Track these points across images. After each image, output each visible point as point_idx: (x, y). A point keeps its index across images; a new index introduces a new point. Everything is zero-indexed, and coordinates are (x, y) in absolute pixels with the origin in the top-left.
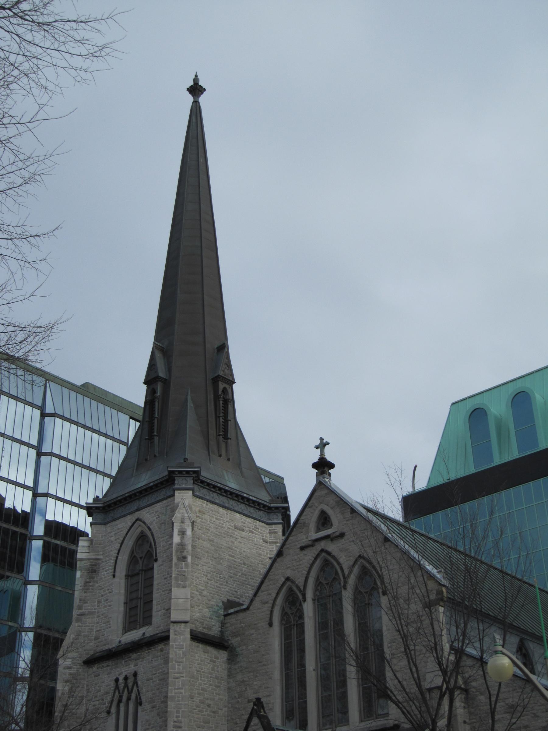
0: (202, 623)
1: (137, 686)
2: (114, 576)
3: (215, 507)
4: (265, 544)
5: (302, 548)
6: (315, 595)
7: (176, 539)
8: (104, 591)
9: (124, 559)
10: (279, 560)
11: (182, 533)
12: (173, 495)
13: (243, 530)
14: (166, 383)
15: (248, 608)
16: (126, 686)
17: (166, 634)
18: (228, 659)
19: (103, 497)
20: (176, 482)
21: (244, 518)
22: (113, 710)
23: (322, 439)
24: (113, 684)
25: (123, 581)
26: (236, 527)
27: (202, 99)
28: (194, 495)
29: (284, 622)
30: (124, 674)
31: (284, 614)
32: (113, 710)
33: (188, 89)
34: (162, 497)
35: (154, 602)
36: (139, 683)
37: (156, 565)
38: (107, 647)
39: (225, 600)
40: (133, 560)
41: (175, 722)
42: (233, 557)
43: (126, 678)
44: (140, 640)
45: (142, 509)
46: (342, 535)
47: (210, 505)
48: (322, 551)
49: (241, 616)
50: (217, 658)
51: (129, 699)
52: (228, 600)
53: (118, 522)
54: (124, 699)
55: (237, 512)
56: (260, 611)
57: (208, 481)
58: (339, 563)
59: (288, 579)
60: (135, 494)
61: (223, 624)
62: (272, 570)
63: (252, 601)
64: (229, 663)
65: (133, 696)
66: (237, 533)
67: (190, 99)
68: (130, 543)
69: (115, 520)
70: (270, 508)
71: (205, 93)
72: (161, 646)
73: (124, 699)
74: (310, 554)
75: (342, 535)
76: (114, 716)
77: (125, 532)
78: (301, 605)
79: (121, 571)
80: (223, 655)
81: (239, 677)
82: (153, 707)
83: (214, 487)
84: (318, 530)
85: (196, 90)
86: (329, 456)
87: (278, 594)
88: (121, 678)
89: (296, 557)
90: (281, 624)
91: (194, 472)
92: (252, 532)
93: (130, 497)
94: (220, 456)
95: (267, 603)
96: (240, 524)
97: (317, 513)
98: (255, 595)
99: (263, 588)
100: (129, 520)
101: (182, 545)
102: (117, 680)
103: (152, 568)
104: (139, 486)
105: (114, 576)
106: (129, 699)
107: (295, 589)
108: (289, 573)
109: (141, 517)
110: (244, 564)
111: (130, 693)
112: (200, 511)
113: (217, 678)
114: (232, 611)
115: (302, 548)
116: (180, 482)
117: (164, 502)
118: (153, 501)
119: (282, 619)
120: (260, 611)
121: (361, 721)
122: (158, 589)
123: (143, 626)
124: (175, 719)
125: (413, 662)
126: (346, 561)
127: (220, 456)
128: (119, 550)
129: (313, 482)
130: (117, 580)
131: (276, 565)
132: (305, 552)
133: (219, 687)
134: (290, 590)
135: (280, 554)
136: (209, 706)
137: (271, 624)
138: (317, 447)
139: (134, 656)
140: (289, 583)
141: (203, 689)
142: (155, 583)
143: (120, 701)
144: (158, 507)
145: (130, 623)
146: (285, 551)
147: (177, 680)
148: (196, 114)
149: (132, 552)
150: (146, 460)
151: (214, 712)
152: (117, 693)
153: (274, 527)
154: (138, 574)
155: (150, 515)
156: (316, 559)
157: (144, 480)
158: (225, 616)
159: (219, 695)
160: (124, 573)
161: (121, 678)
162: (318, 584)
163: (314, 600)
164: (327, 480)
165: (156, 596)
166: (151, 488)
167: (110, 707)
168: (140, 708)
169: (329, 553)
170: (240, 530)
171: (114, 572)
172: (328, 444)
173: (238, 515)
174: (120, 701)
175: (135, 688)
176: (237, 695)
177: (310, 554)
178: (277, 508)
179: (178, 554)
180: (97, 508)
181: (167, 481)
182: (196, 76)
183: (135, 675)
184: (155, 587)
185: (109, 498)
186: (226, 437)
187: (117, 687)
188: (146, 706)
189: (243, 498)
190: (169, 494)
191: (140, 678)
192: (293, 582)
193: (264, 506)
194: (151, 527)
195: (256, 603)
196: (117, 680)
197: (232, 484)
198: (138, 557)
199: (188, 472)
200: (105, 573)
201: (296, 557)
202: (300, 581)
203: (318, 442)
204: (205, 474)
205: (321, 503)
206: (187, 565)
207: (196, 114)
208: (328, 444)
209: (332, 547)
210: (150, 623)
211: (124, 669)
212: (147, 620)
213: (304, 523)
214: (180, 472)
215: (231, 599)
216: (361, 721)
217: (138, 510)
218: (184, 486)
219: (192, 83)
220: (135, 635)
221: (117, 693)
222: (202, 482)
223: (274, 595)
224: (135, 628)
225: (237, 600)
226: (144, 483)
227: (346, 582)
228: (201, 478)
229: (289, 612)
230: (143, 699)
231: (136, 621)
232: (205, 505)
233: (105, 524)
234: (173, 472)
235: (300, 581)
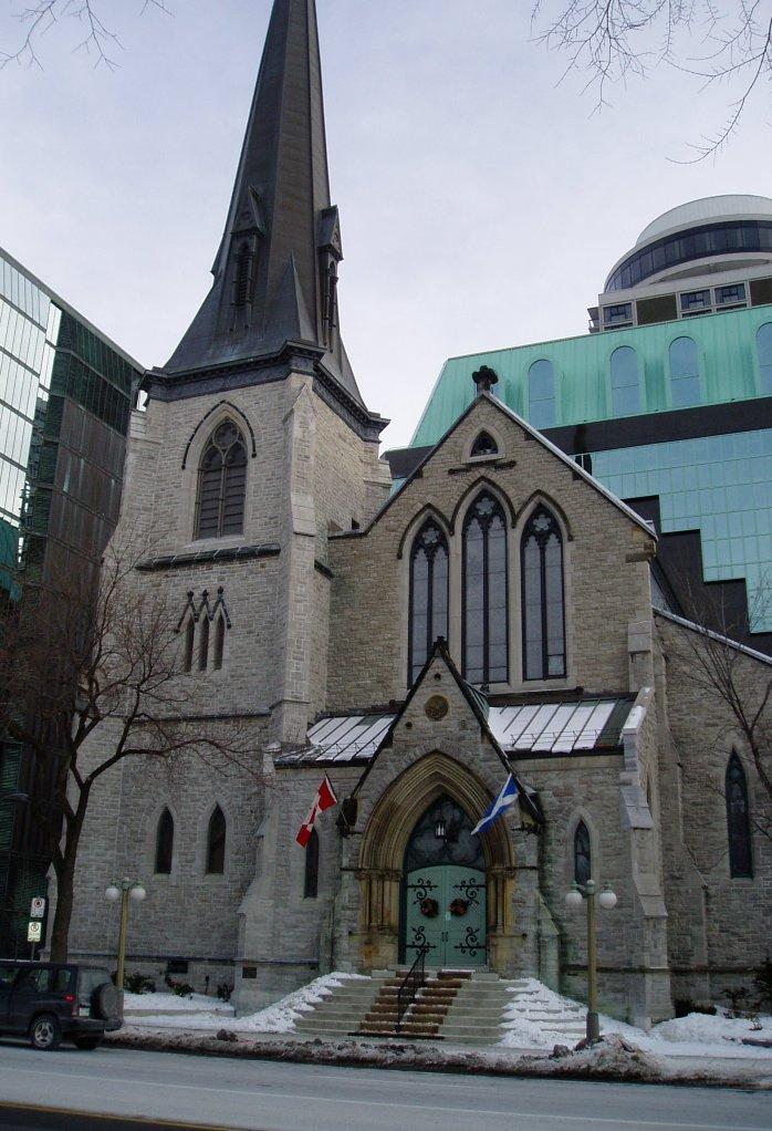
2: (183, 467)
5: (452, 472)
8: (167, 484)
9: (197, 449)
14: (264, 240)
15: (364, 534)
16: (205, 602)
32: (183, 629)
34: (264, 379)
36: (226, 602)
43: (205, 594)
45: (739, 268)
46: (512, 464)
56: (383, 540)
59: (429, 506)
63: (372, 525)
64: (332, 595)
74: (463, 482)
75: (512, 464)
76: (184, 636)
79: (194, 463)
81: (348, 613)
82: (249, 632)
84: (474, 453)
87: (412, 522)
88: (197, 594)
93: (212, 372)
96: (342, 433)
97: (476, 432)
98: (378, 519)
100: (216, 399)
102: (191, 595)
108: (430, 499)
115: (452, 472)
116: (296, 363)
118: (249, 381)
120: (383, 540)
124: (296, 650)
129: (472, 396)
130: (186, 473)
137: (400, 556)
147: (299, 604)
150: (231, 330)
156: (471, 487)
160: (196, 466)
161: (197, 594)
166: (248, 364)
171: (184, 462)
177: (463, 482)
180: (160, 379)
183: (221, 591)
185: (644, 239)
191: (225, 596)
194: (245, 413)
209: (494, 475)
212: (235, 524)
221: (190, 610)
233: (167, 401)
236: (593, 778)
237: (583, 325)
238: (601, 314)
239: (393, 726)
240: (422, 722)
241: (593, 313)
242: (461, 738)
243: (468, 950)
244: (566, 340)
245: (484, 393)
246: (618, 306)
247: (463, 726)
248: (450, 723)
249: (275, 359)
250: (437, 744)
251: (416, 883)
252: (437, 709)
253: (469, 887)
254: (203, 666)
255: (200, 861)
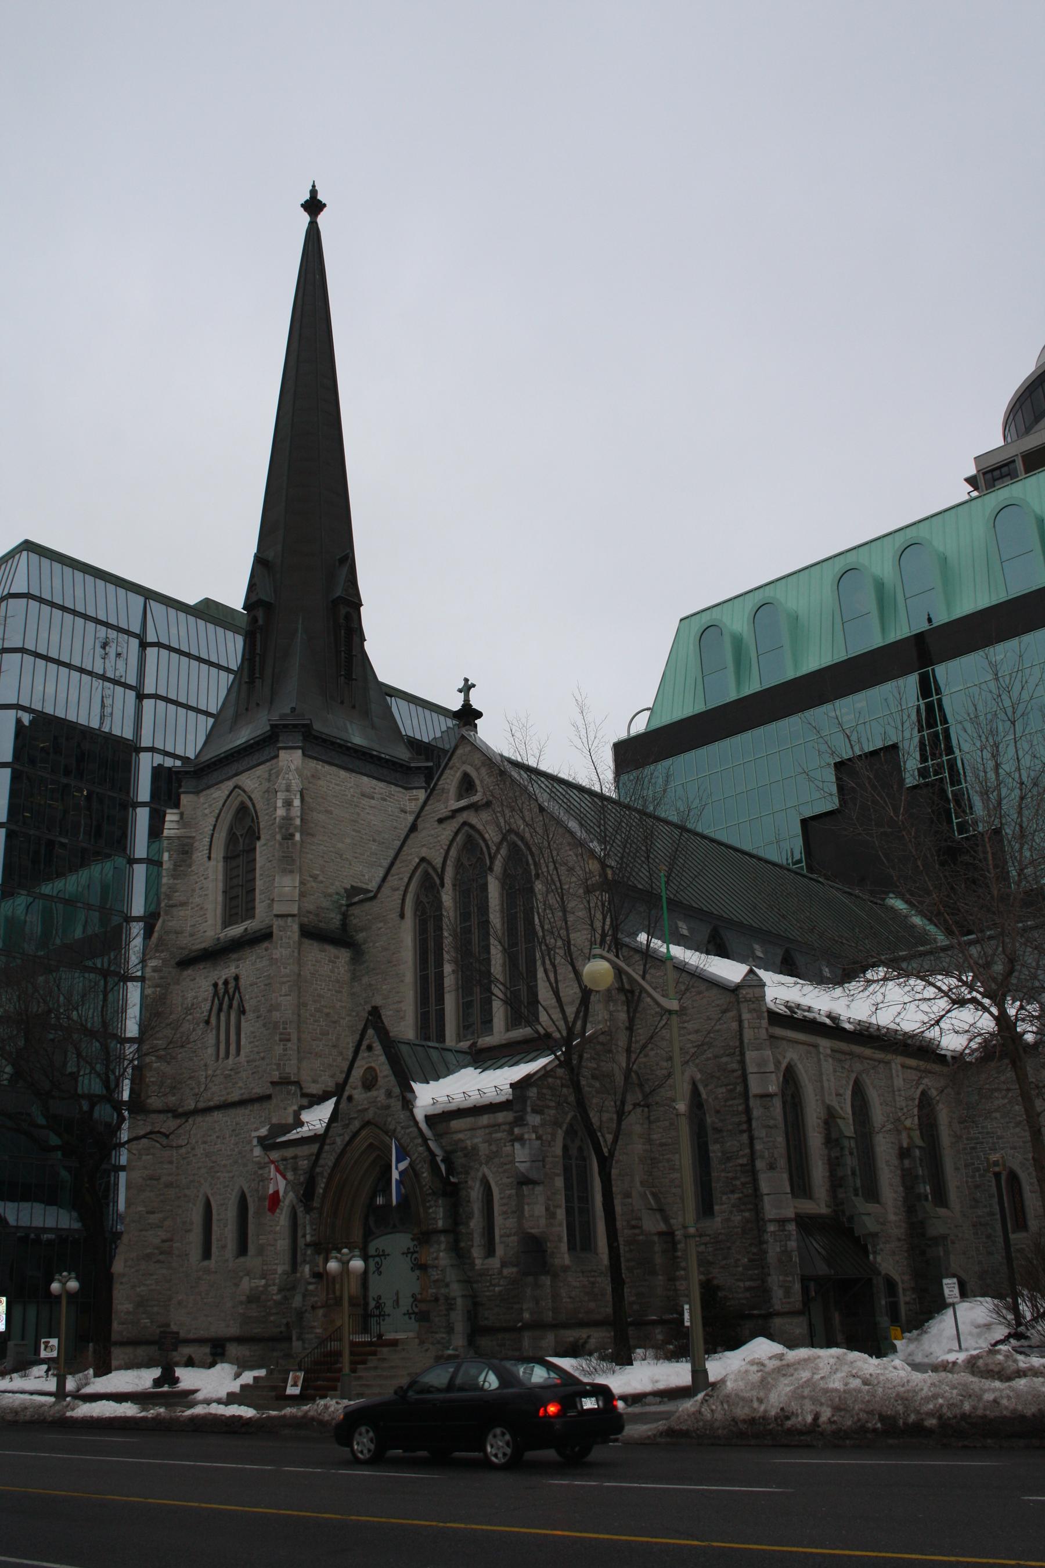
0: (317, 915)
1: (240, 993)
2: (209, 858)
3: (334, 768)
4: (403, 815)
6: (455, 879)
7: (281, 812)
9: (221, 837)
10: (412, 835)
11: (288, 804)
12: (277, 756)
13: (373, 798)
15: (375, 897)
16: (226, 991)
17: (268, 931)
18: (352, 959)
19: (197, 757)
20: (281, 738)
21: (374, 782)
22: (213, 1020)
23: (466, 680)
24: (211, 989)
25: (221, 865)
26: (363, 795)
27: (321, 219)
28: (304, 754)
29: (418, 913)
30: (224, 977)
31: (418, 904)
33: (302, 205)
35: (257, 891)
36: (242, 990)
37: (258, 844)
38: (203, 946)
39: (349, 887)
40: (232, 838)
41: (281, 1034)
42: (359, 832)
44: (242, 937)
47: (327, 767)
48: (465, 824)
49: (367, 905)
50: (338, 958)
51: (230, 1006)
52: (352, 886)
53: (212, 790)
54: (225, 1006)
55: (365, 775)
56: (390, 899)
57: (324, 736)
58: (484, 840)
59: (423, 860)
60: (232, 755)
61: (345, 916)
62: (405, 848)
65: (235, 1003)
66: (365, 801)
67: (306, 218)
68: (228, 817)
69: (209, 787)
70: (409, 768)
71: (325, 209)
72: (265, 944)
73: (225, 1006)
77: (221, 802)
78: (438, 892)
79: (218, 853)
80: (344, 956)
81: (365, 980)
83: (333, 743)
84: (460, 797)
85: (313, 206)
86: (476, 704)
88: (220, 983)
89: (432, 832)
90: (415, 915)
91: (304, 725)
92: (385, 800)
93: (226, 758)
94: (342, 703)
95: (398, 889)
97: (459, 774)
99: (393, 871)
101: (288, 819)
102: (215, 985)
103: (255, 849)
104: (239, 742)
105: (209, 858)
106: (230, 1006)
107: (431, 871)
108: (424, 852)
109: (240, 784)
110: (374, 841)
111: (231, 1000)
112: (313, 776)
113: (338, 981)
114: (356, 899)
115: (440, 821)
117: (268, 764)
119: (416, 910)
121: (508, 1030)
122: (261, 875)
123: (245, 920)
125: (550, 959)
126: (492, 835)
127: (342, 703)
128: (215, 826)
130: (212, 863)
131: (409, 842)
132: (443, 826)
133: (340, 992)
134: (426, 874)
135: (413, 828)
136: (328, 1015)
137: (402, 916)
138: (460, 691)
139: (234, 956)
140: (424, 865)
141: (319, 996)
142: (258, 866)
143: (220, 1010)
144: (261, 770)
145: (230, 917)
146: (420, 825)
148: (313, 241)
149: (231, 829)
151: (335, 1022)
152: (216, 1001)
153: (415, 792)
154: (238, 856)
155: (251, 781)
156: (456, 834)
157: (243, 736)
158: (348, 906)
159: (341, 1001)
161: (220, 983)
162: (459, 865)
163: (454, 885)
164: (472, 733)
165: (259, 884)
166: (251, 746)
167: (209, 1016)
168: (242, 1017)
169: (472, 826)
170: (368, 797)
171: (210, 853)
172: (474, 686)
173: (365, 778)
174: (220, 1010)
175: (237, 995)
176: (362, 1002)
178: (419, 768)
179: (283, 830)
180: (187, 772)
181: (270, 737)
182: (314, 186)
183: (237, 978)
184: (258, 872)
186: (349, 677)
187: (216, 993)
188: (250, 1015)
189: (372, 756)
190: (273, 754)
192: (429, 863)
193: (402, 766)
194: (253, 796)
195: (386, 890)
196: (215, 985)
197: (358, 739)
198: (238, 834)
199: (295, 726)
200: (199, 855)
201: (432, 832)
202: (438, 862)
203: (461, 684)
204: (317, 726)
205: (464, 763)
206: (294, 844)
207: (313, 241)
208: (474, 686)
210: (253, 917)
211: (225, 972)
212: (250, 912)
213: (443, 789)
214: (285, 726)
215: (354, 884)
216: (508, 1030)
217: (236, 775)
218: (291, 744)
219: (307, 197)
220: (236, 931)
221: (216, 1001)
222: (316, 738)
223: (406, 880)
224: (236, 923)
225: (365, 886)
226: (243, 740)
227: (492, 863)
228: (314, 733)
229: (425, 900)
230: (247, 1008)
231: (237, 914)
232: (319, 767)
234: (276, 726)
235: (438, 862)
236: (494, 1135)
237: (963, 492)
238: (981, 482)
239: (337, 1104)
240: (359, 1095)
241: (971, 481)
242: (388, 1107)
243: (413, 1316)
244: (884, 536)
245: (464, 732)
246: (1000, 468)
247: (389, 1094)
248: (379, 1094)
249: (264, 740)
250: (369, 1115)
251: (375, 1253)
252: (370, 1082)
253: (413, 1253)
254: (227, 1056)
255: (231, 1245)
